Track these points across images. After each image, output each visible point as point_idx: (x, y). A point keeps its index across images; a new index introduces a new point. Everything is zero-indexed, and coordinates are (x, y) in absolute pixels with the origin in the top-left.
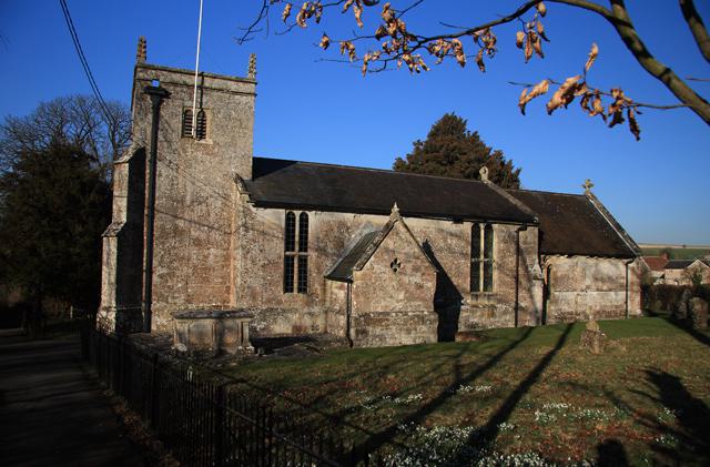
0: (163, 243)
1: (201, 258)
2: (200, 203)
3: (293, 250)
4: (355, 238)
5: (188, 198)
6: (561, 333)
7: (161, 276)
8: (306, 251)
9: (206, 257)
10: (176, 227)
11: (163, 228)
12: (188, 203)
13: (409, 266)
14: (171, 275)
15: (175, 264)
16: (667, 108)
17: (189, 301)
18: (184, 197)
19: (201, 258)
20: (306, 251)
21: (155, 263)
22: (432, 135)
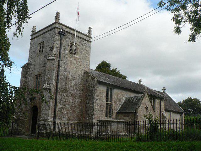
0: (61, 94)
1: (73, 102)
2: (74, 80)
3: (110, 104)
4: (139, 98)
5: (70, 77)
6: (172, 113)
7: (60, 108)
8: (106, 103)
9: (75, 102)
10: (66, 88)
11: (61, 88)
12: (70, 79)
13: (74, 125)
14: (63, 108)
15: (65, 104)
16: (44, 7)
17: (68, 119)
18: (69, 77)
19: (73, 102)
20: (106, 103)
21: (58, 102)
22: (194, 99)
